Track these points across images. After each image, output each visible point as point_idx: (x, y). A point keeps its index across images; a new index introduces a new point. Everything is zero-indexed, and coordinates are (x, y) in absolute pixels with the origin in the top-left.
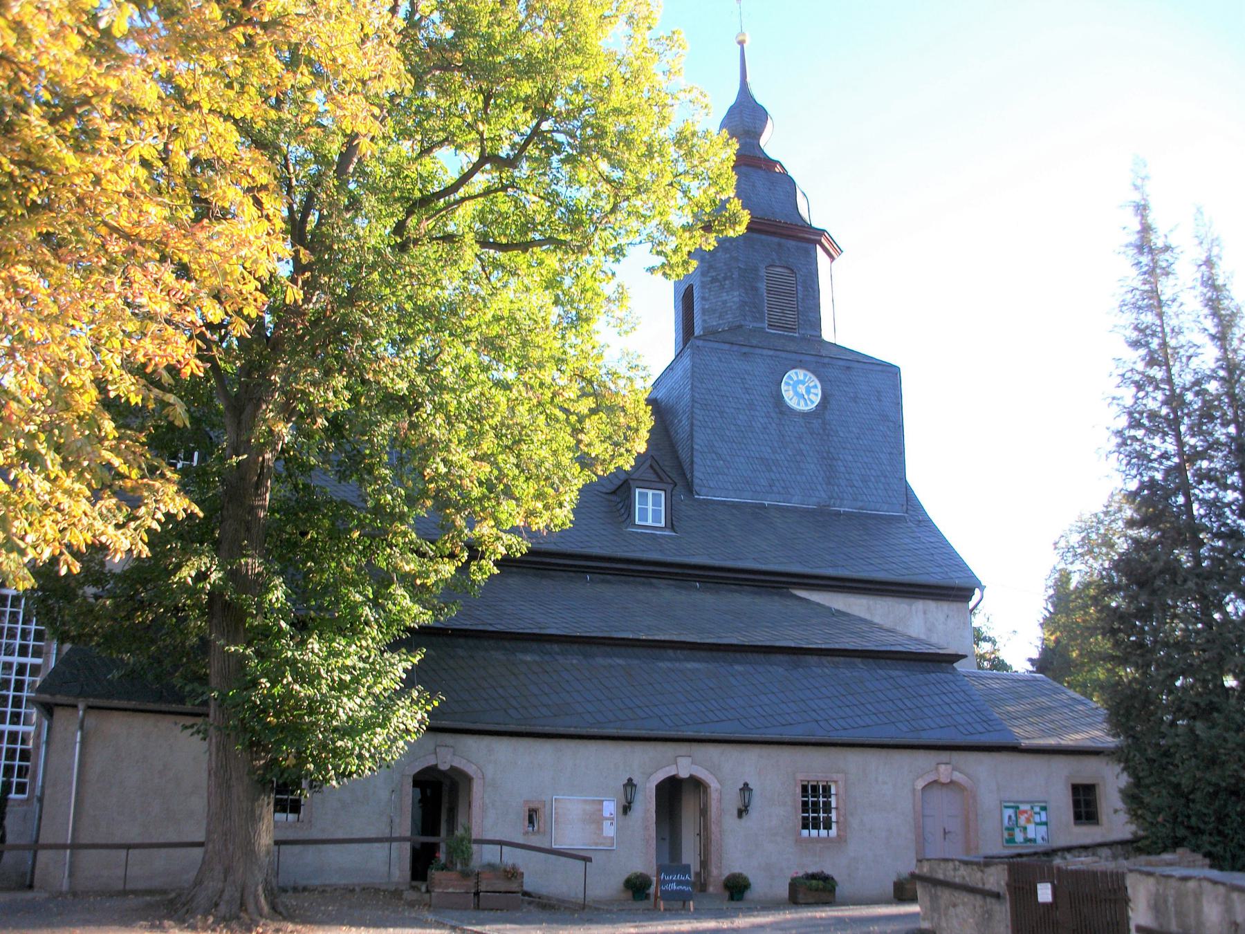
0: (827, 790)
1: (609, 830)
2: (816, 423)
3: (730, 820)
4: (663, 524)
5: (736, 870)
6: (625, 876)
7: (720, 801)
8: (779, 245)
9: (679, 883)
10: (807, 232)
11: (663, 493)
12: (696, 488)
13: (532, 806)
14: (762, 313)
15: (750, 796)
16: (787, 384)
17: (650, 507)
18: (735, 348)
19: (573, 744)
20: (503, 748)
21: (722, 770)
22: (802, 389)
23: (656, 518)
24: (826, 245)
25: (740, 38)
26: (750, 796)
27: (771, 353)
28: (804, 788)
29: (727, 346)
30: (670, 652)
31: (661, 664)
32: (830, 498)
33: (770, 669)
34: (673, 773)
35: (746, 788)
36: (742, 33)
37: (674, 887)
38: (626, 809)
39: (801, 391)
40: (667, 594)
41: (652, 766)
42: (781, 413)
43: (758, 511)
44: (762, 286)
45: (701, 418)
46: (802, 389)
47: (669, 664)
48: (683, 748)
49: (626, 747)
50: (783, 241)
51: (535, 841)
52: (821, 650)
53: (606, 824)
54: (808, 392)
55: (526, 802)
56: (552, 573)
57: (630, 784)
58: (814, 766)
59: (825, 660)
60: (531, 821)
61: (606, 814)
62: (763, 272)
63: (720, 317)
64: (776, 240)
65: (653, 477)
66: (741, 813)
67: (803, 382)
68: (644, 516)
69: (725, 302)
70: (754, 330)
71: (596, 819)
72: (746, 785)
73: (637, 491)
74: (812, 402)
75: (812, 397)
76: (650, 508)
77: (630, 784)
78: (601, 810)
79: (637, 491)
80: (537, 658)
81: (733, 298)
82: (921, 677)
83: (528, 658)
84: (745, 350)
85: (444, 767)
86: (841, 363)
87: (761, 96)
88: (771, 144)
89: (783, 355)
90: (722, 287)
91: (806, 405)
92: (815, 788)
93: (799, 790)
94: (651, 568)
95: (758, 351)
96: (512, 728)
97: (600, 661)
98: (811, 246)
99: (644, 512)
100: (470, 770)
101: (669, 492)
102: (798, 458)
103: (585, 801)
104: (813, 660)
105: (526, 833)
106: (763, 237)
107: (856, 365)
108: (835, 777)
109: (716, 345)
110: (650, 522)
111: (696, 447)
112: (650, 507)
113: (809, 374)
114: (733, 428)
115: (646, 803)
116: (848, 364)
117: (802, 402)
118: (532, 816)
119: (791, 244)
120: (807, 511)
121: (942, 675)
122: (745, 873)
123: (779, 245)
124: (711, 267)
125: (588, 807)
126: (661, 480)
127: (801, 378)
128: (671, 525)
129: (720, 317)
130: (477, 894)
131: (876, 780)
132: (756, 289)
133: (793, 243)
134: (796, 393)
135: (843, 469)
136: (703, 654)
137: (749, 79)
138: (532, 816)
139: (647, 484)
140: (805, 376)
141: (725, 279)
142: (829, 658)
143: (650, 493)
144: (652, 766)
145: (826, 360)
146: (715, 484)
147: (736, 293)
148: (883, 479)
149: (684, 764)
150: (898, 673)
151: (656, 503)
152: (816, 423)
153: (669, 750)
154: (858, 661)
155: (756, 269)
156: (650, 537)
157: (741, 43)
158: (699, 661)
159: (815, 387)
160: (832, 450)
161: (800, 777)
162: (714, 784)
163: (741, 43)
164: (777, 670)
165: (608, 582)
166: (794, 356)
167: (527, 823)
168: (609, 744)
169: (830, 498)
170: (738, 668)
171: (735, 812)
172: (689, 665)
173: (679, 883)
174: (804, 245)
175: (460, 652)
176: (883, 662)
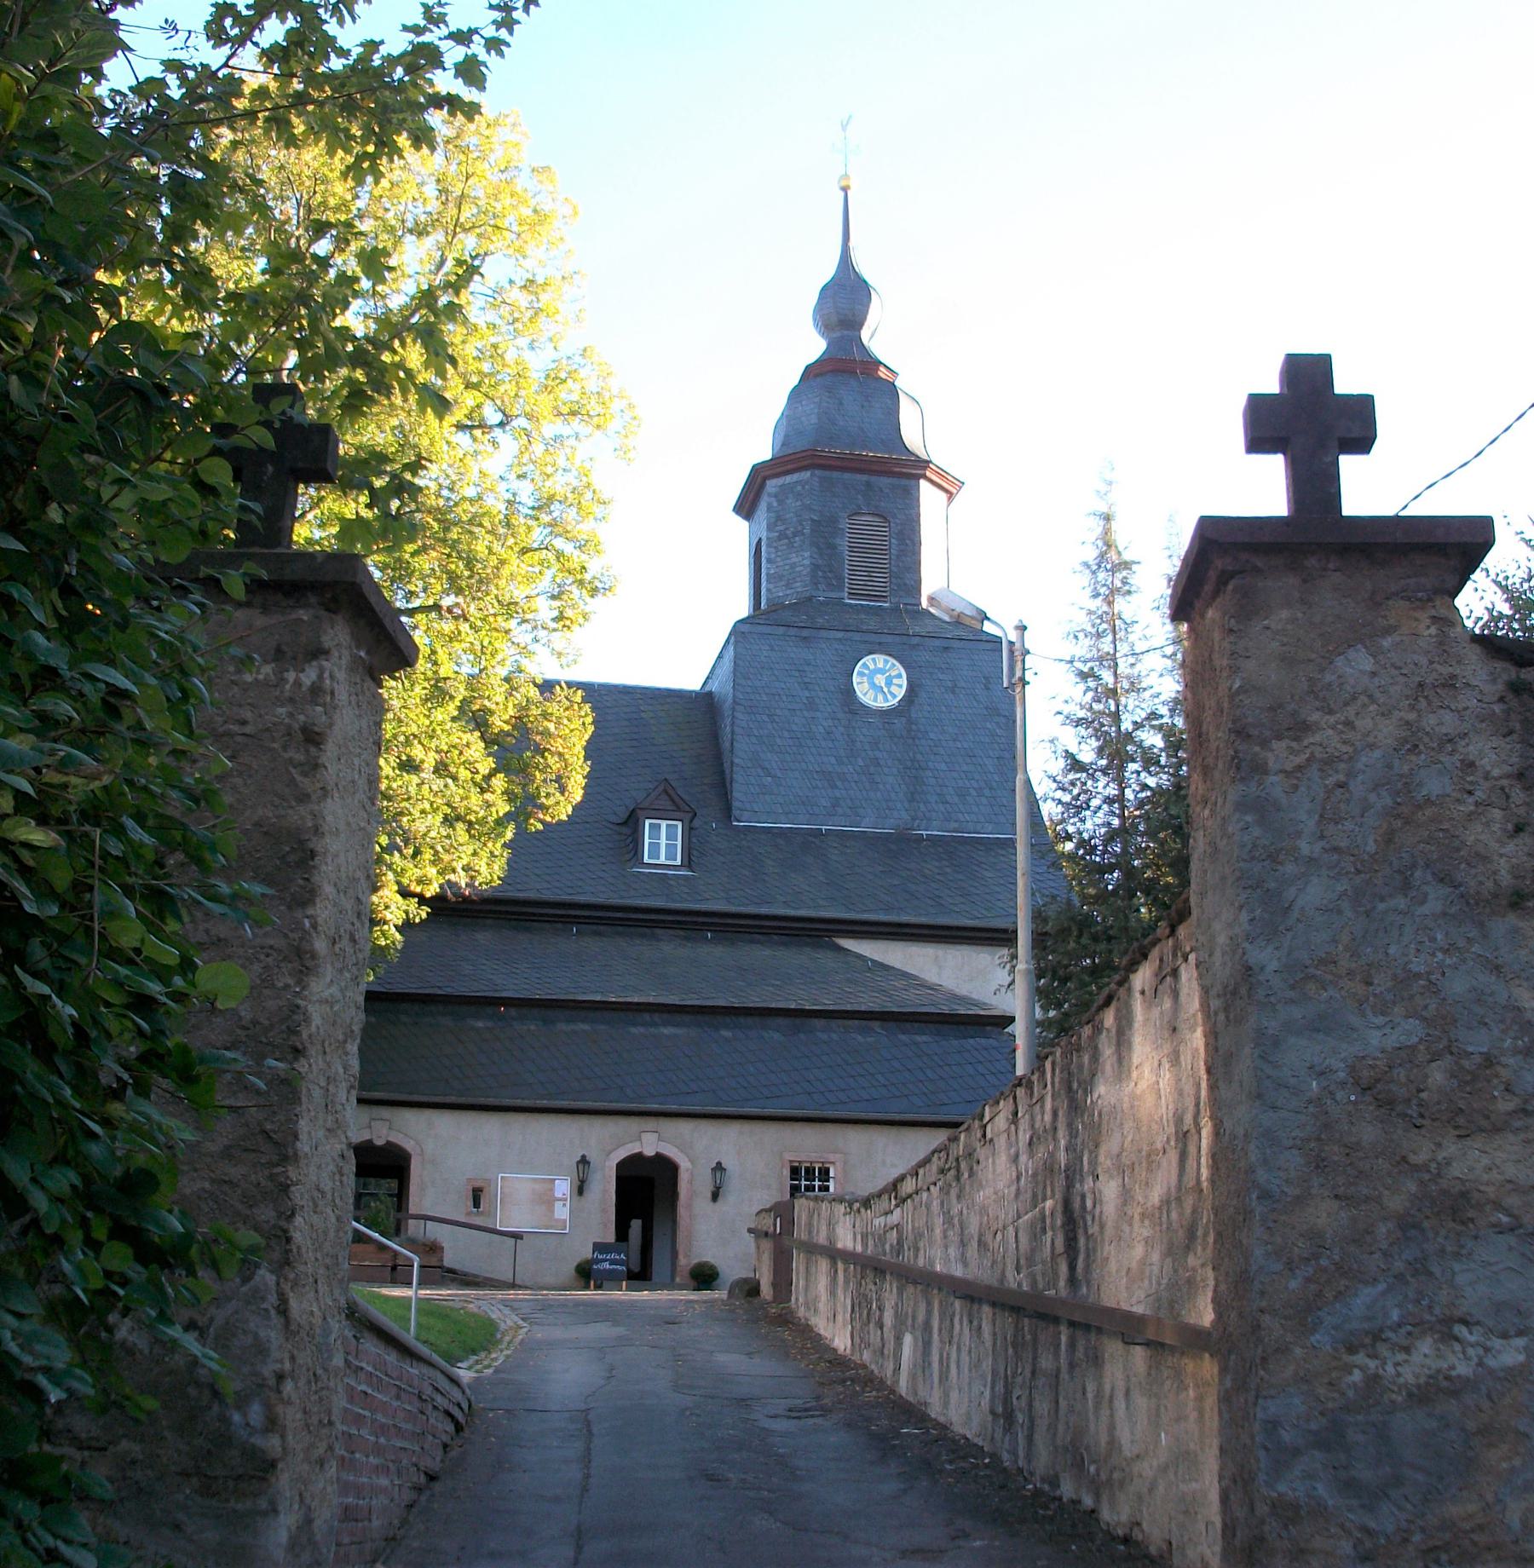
0: (824, 1175)
1: (562, 1212)
2: (899, 723)
3: (702, 1204)
4: (679, 862)
5: (708, 1258)
6: (578, 1260)
7: (690, 1182)
8: (868, 484)
9: (613, 1262)
10: (905, 466)
11: (680, 824)
12: (735, 812)
13: (478, 1184)
14: (840, 579)
15: (731, 1177)
16: (861, 674)
17: (663, 841)
18: (793, 631)
19: (521, 1118)
20: (445, 1122)
21: (691, 1147)
22: (880, 680)
23: (671, 855)
24: (934, 478)
25: (843, 183)
26: (731, 1177)
27: (840, 635)
28: (795, 1172)
29: (781, 630)
30: (647, 1016)
31: (633, 1030)
32: (914, 819)
33: (765, 1034)
34: (368, 1137)
35: (719, 1167)
36: (846, 176)
37: (607, 1265)
38: (581, 1190)
39: (879, 682)
40: (671, 950)
41: (611, 1143)
42: (853, 713)
43: (811, 841)
44: (843, 544)
45: (744, 724)
46: (880, 680)
47: (642, 1030)
48: (651, 1123)
49: (583, 1122)
50: (873, 479)
51: (478, 1221)
52: (847, 1012)
53: (558, 1205)
54: (889, 683)
55: (469, 1180)
56: (528, 924)
57: (584, 1161)
58: (807, 1144)
59: (834, 1023)
60: (477, 1204)
61: (558, 1194)
62: (844, 524)
63: (788, 586)
64: (864, 478)
65: (668, 805)
66: (715, 1196)
67: (881, 671)
68: (655, 851)
69: (793, 566)
70: (828, 602)
71: (548, 1200)
72: (719, 1164)
73: (647, 822)
74: (894, 696)
75: (894, 689)
76: (662, 843)
77: (584, 1161)
78: (552, 1190)
79: (647, 822)
80: (490, 1024)
81: (803, 559)
82: (955, 1042)
83: (480, 1024)
84: (805, 633)
85: (379, 1142)
86: (937, 643)
87: (864, 266)
88: (881, 336)
89: (857, 637)
90: (791, 545)
91: (886, 700)
92: (810, 1172)
93: (787, 1172)
94: (653, 917)
95: (824, 633)
96: (452, 1099)
97: (563, 1026)
98: (913, 482)
99: (655, 848)
100: (408, 1145)
101: (687, 821)
102: (872, 769)
103: (535, 1180)
104: (818, 1023)
105: (469, 1214)
106: (847, 476)
107: (956, 644)
108: (831, 1157)
109: (768, 630)
110: (662, 860)
111: (736, 761)
112: (663, 841)
113: (892, 660)
114: (786, 734)
115: (604, 1188)
116: (945, 643)
117: (880, 697)
118: (477, 1196)
119: (884, 481)
120: (879, 836)
121: (983, 1041)
122: (713, 1261)
123: (868, 484)
124: (779, 518)
125: (537, 1186)
126: (679, 809)
127: (880, 665)
128: (688, 862)
129: (788, 586)
130: (394, 1268)
131: (884, 1162)
132: (833, 547)
133: (890, 480)
134: (873, 685)
135: (932, 781)
136: (687, 1018)
137: (852, 244)
138: (477, 1196)
139: (658, 814)
140: (886, 662)
141: (795, 535)
142: (840, 1022)
143: (664, 824)
144: (611, 1143)
145: (916, 640)
146: (759, 808)
147: (807, 554)
148: (987, 792)
149: (649, 1141)
150: (924, 1038)
151: (671, 836)
152: (899, 723)
153: (633, 1124)
154: (876, 1025)
155: (833, 521)
156: (662, 880)
157: (845, 189)
158: (677, 1025)
159: (899, 676)
160: (919, 757)
161: (789, 1156)
162: (684, 1164)
163: (845, 189)
164: (774, 1035)
165: (600, 934)
166: (873, 638)
167: (470, 1203)
168: (797, 1126)
169: (914, 819)
170: (726, 1033)
171: (709, 1195)
172: (666, 1031)
173: (613, 1262)
174: (904, 482)
175: (404, 1018)
176: (908, 1025)
